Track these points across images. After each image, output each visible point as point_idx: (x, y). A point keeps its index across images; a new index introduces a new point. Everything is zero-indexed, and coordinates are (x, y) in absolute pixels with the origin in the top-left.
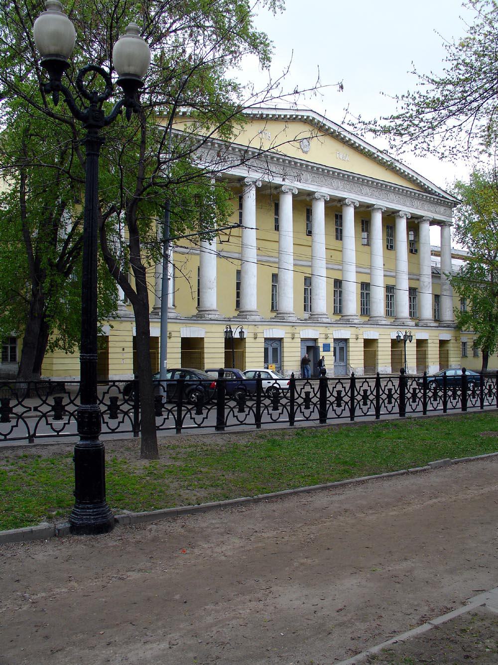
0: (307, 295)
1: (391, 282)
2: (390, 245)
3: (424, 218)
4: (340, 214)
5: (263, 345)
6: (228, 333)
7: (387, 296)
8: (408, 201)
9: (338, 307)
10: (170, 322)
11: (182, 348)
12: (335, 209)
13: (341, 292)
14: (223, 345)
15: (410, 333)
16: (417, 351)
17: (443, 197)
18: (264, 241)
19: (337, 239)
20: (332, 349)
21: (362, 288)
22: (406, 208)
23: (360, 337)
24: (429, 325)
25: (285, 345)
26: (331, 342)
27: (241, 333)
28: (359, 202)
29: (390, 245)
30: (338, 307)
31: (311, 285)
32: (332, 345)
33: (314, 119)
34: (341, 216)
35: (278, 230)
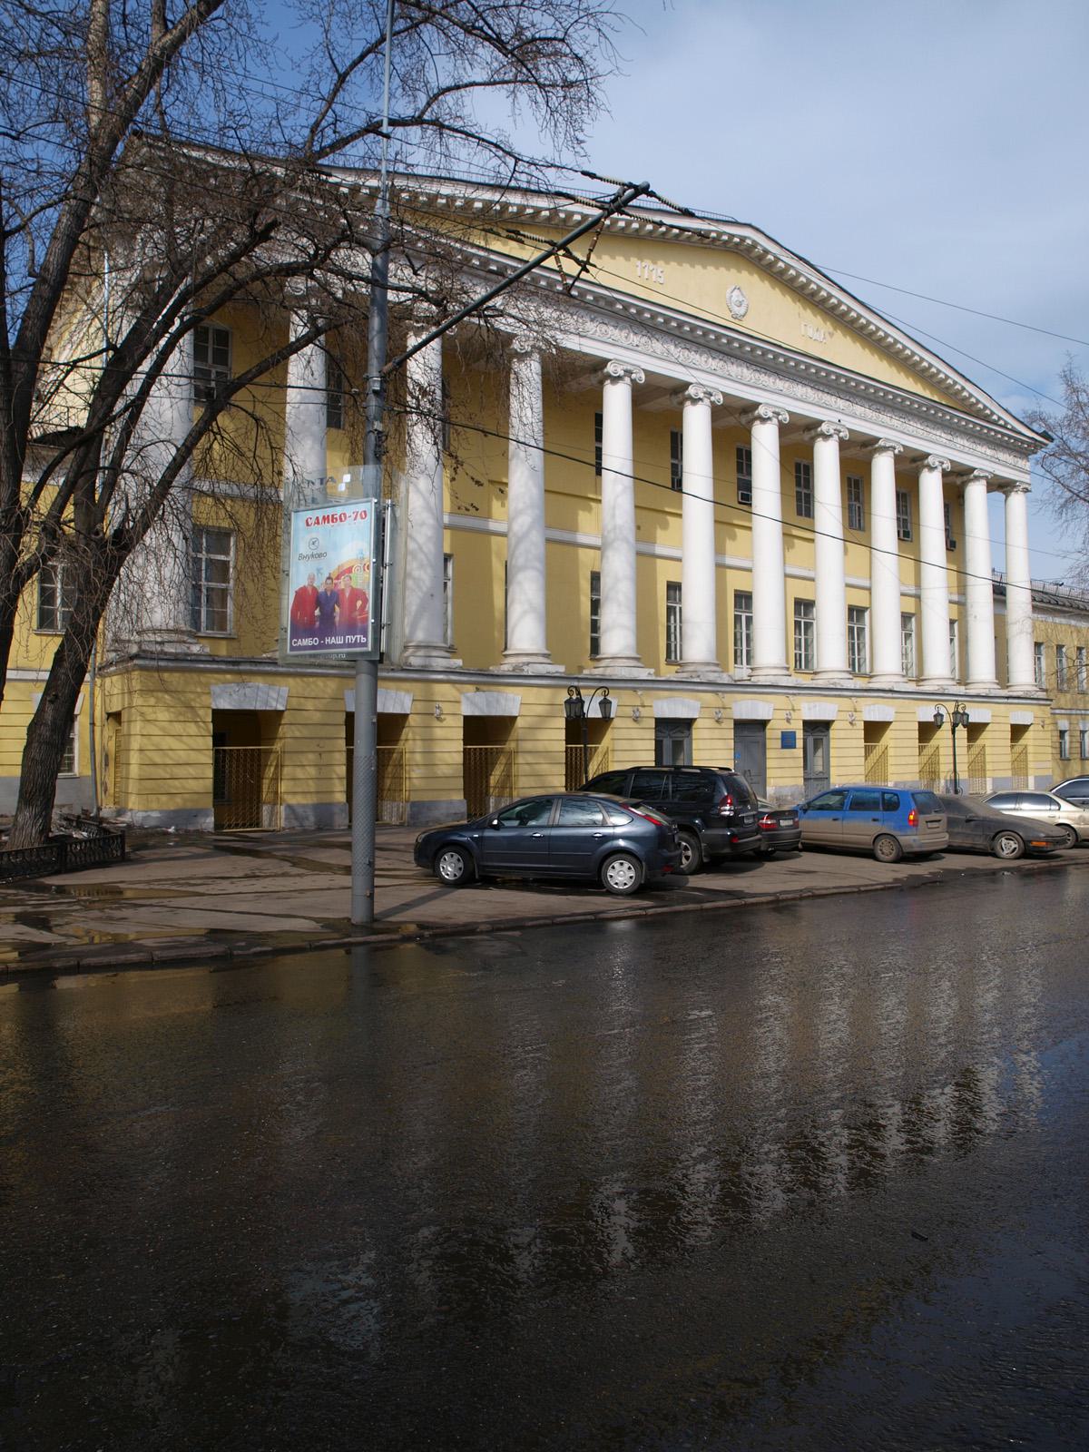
0: (738, 629)
1: (859, 599)
2: (908, 530)
3: (976, 473)
4: (805, 462)
5: (652, 734)
6: (575, 705)
7: (851, 630)
8: (942, 436)
9: (803, 657)
10: (385, 679)
11: (466, 741)
12: (658, 409)
13: (749, 620)
14: (563, 736)
15: (964, 708)
16: (465, 751)
17: (1013, 430)
18: (561, 497)
19: (799, 513)
20: (800, 743)
21: (850, 618)
22: (944, 449)
23: (794, 715)
24: (529, 670)
25: (695, 733)
26: (797, 727)
27: (605, 704)
28: (952, 461)
29: (908, 530)
30: (803, 657)
31: (680, 600)
32: (800, 734)
33: (755, 244)
34: (749, 454)
35: (860, 528)
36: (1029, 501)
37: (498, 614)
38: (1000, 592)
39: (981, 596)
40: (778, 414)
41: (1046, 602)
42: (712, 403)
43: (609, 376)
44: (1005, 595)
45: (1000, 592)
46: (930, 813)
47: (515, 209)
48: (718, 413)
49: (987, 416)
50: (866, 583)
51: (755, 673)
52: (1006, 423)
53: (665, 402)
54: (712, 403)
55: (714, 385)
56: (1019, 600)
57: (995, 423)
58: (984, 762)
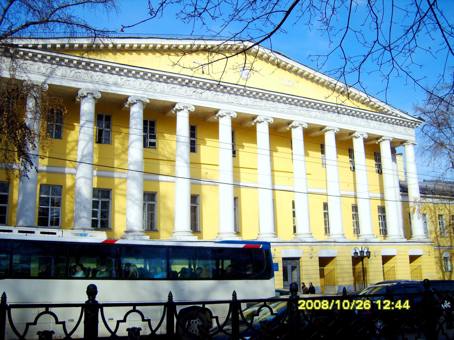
8: (386, 126)
17: (401, 117)
36: (415, 148)
37: (242, 246)
38: (404, 189)
39: (392, 193)
40: (230, 113)
41: (424, 191)
42: (269, 123)
43: (220, 116)
44: (407, 192)
45: (404, 189)
46: (11, 226)
47: (120, 46)
48: (337, 136)
49: (386, 112)
50: (324, 191)
51: (260, 236)
52: (397, 115)
53: (318, 133)
54: (269, 123)
55: (267, 115)
56: (414, 193)
57: (390, 115)
58: (421, 273)
